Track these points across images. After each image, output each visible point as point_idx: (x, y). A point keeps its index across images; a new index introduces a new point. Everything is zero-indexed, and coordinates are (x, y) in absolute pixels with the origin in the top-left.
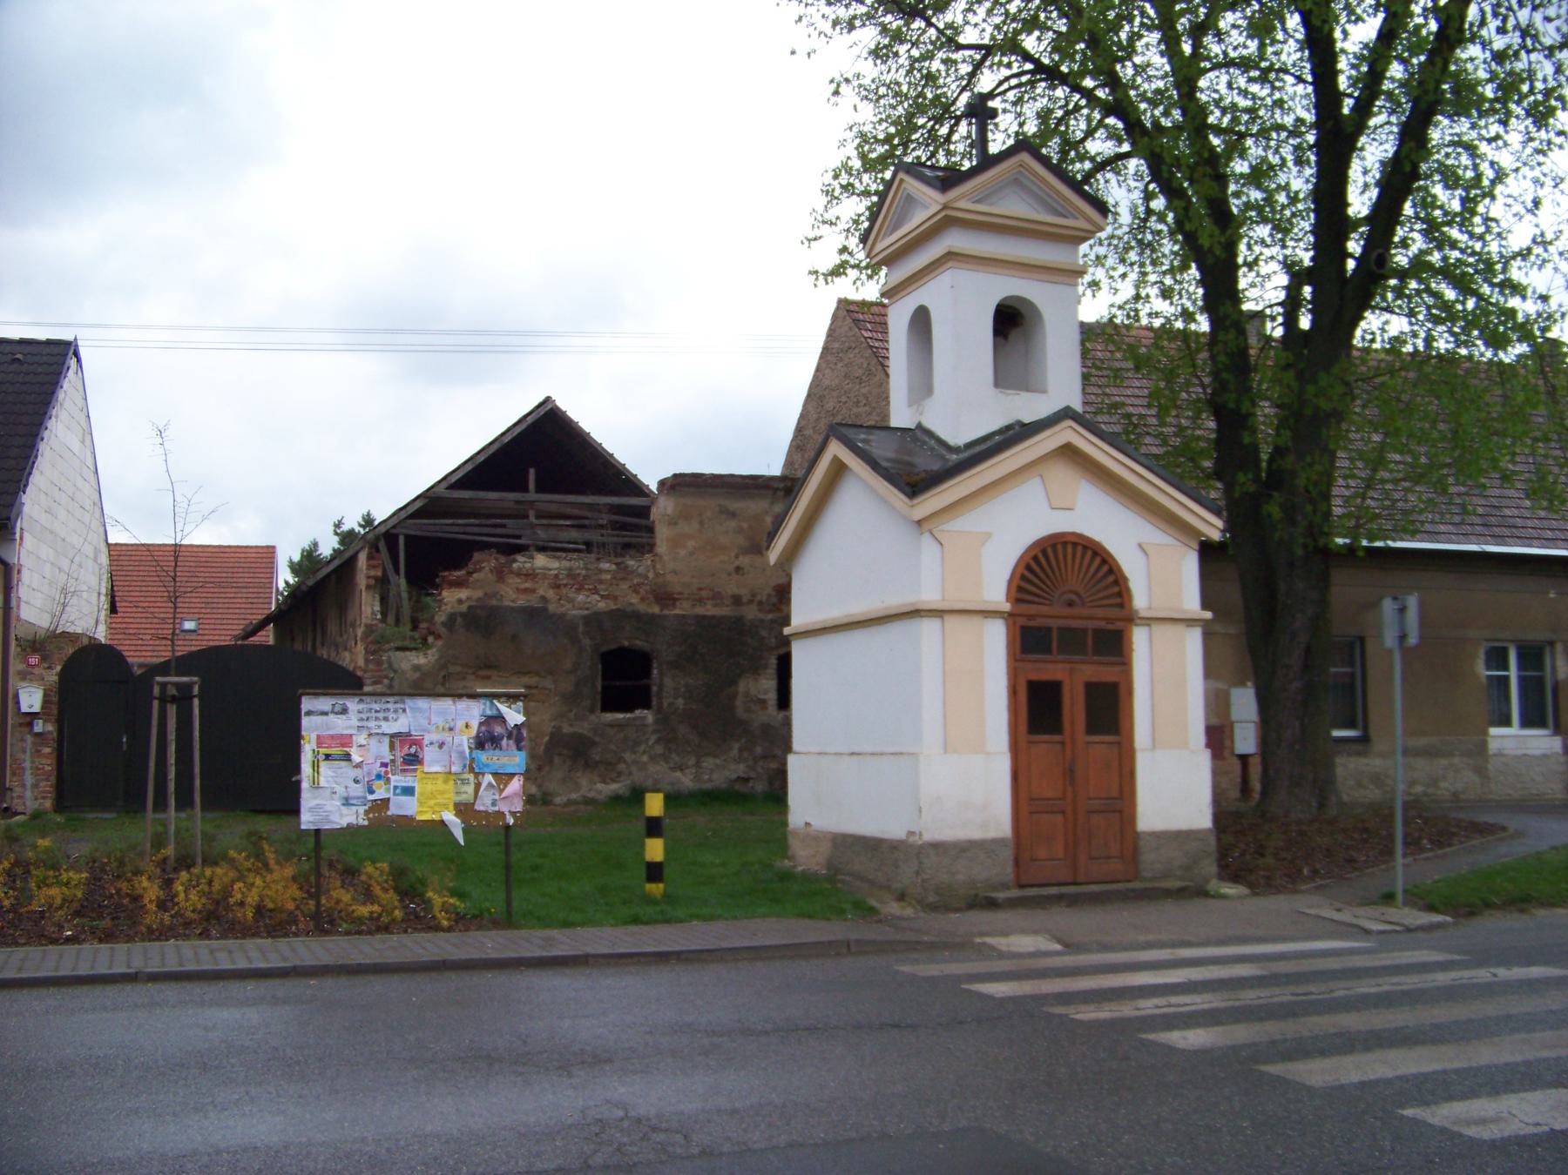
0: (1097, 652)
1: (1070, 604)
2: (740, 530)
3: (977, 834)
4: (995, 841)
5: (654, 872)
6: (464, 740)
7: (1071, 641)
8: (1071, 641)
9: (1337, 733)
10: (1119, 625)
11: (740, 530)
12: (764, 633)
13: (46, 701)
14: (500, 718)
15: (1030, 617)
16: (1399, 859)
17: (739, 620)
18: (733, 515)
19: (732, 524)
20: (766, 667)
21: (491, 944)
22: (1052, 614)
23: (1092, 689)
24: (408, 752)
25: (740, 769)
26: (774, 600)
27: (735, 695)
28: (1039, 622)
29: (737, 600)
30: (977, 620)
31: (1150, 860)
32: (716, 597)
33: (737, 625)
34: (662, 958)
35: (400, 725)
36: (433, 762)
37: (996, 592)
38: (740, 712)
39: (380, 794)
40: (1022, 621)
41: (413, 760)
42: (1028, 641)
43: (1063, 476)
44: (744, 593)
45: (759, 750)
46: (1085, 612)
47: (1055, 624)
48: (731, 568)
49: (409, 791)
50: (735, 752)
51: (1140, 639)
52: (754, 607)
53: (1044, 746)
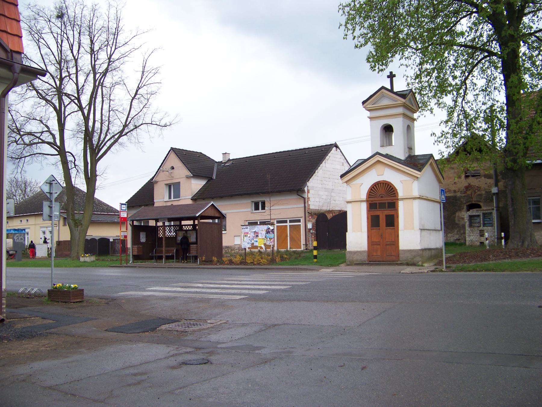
0: (388, 208)
1: (382, 197)
2: (455, 173)
3: (359, 250)
4: (363, 251)
5: (315, 257)
6: (264, 232)
7: (382, 206)
8: (382, 206)
9: (533, 221)
10: (394, 201)
11: (455, 173)
12: (462, 200)
13: (313, 226)
14: (269, 228)
15: (372, 201)
16: (164, 249)
17: (455, 197)
18: (453, 168)
19: (452, 171)
20: (463, 209)
21: (229, 266)
22: (377, 200)
23: (387, 216)
24: (257, 235)
25: (457, 237)
26: (465, 190)
27: (455, 217)
28: (374, 202)
29: (455, 191)
30: (411, 200)
31: (402, 257)
32: (450, 191)
33: (455, 198)
34: (266, 269)
35: (254, 230)
36: (260, 237)
37: (364, 196)
38: (457, 222)
39: (253, 242)
40: (370, 202)
41: (257, 236)
42: (372, 206)
43: (379, 167)
44: (456, 189)
45: (462, 232)
46: (385, 198)
47: (378, 202)
48: (453, 183)
49: (257, 241)
50: (456, 232)
51: (401, 204)
52: (459, 193)
53: (375, 231)
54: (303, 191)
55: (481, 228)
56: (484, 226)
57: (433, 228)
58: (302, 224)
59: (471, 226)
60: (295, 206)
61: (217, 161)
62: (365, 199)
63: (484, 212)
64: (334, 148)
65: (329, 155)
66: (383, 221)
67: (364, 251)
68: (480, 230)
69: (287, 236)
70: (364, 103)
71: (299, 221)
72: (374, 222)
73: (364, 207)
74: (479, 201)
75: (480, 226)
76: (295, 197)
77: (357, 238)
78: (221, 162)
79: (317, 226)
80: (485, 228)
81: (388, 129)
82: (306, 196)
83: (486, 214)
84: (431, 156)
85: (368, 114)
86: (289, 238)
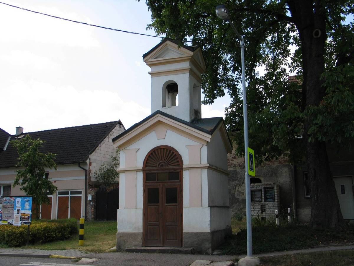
37: (140, 165)
54: (85, 163)
55: (262, 203)
56: (265, 201)
57: (222, 205)
58: (83, 196)
59: (252, 199)
60: (77, 178)
61: (12, 134)
62: (141, 168)
63: (266, 186)
64: (118, 125)
65: (113, 131)
66: (162, 196)
67: (138, 234)
68: (261, 205)
69: (68, 208)
70: (145, 56)
71: (80, 193)
72: (151, 196)
73: (140, 176)
74: (260, 176)
75: (262, 201)
76: (76, 169)
77: (131, 213)
78: (15, 135)
79: (96, 198)
80: (267, 203)
81: (172, 88)
82: (88, 169)
83: (267, 188)
84: (222, 118)
85: (149, 69)
86: (69, 209)
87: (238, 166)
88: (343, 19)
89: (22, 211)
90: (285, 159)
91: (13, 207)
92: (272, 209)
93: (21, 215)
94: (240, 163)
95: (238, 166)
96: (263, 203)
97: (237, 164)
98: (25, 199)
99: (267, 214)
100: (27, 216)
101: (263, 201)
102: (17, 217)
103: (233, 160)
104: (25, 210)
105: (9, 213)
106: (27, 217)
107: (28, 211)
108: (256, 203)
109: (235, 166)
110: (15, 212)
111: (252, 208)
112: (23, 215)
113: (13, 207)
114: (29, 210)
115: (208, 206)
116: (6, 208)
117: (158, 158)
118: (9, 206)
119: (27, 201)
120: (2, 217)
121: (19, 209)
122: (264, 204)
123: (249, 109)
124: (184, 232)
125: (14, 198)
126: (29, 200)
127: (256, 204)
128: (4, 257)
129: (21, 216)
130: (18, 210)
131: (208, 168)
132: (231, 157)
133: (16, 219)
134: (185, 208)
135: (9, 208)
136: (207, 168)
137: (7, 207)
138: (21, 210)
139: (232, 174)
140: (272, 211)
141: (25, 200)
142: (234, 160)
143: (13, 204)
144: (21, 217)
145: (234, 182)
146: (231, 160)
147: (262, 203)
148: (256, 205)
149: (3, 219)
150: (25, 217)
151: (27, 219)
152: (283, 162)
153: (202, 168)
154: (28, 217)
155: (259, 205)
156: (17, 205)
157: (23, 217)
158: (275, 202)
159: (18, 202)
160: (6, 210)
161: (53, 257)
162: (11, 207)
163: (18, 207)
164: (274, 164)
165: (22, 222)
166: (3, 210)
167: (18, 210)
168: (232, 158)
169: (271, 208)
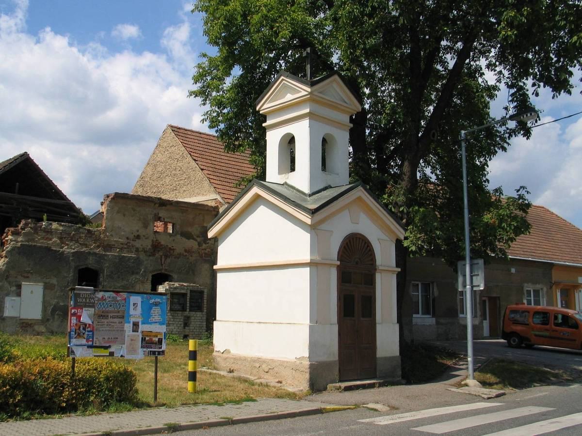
56: (190, 311)
67: (335, 361)
73: (334, 274)
87: (142, 251)
88: (367, 89)
89: (143, 325)
90: (207, 252)
91: (123, 317)
92: (199, 323)
93: (143, 335)
94: (146, 247)
95: (142, 251)
96: (187, 313)
97: (141, 247)
98: (151, 298)
99: (192, 330)
100: (157, 336)
101: (188, 310)
102: (132, 340)
103: (135, 241)
104: (151, 323)
105: (111, 330)
106: (157, 339)
107: (160, 326)
108: (178, 312)
109: (137, 250)
110: (128, 327)
111: (172, 320)
112: (148, 336)
113: (123, 317)
114: (161, 323)
115: (396, 322)
116: (106, 317)
117: (350, 250)
118: (112, 315)
119: (156, 304)
120: (93, 339)
121: (138, 322)
122: (188, 315)
123: (374, 192)
124: (377, 356)
125: (125, 296)
126: (161, 301)
127: (178, 314)
128: (249, 425)
129: (142, 338)
130: (136, 325)
131: (311, 264)
132: (133, 235)
133: (131, 344)
134: (378, 323)
135: (112, 317)
136: (336, 266)
137: (108, 316)
138: (143, 323)
139: (133, 263)
140: (198, 326)
141: (152, 301)
142: (137, 240)
143: (122, 308)
144: (143, 339)
145: (134, 276)
146: (133, 240)
147: (185, 313)
148: (177, 316)
149: (97, 345)
150: (151, 339)
151: (156, 343)
152: (203, 255)
153: (331, 265)
154: (159, 339)
155: (181, 316)
156: (132, 312)
157: (147, 338)
158: (204, 313)
159: (134, 304)
160: (106, 323)
161: (327, 410)
162: (118, 317)
163: (134, 316)
164: (191, 256)
165: (145, 349)
166: (96, 323)
167: (136, 325)
168: (134, 236)
169: (198, 321)
